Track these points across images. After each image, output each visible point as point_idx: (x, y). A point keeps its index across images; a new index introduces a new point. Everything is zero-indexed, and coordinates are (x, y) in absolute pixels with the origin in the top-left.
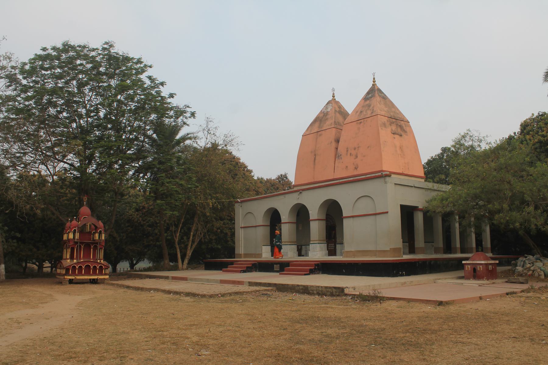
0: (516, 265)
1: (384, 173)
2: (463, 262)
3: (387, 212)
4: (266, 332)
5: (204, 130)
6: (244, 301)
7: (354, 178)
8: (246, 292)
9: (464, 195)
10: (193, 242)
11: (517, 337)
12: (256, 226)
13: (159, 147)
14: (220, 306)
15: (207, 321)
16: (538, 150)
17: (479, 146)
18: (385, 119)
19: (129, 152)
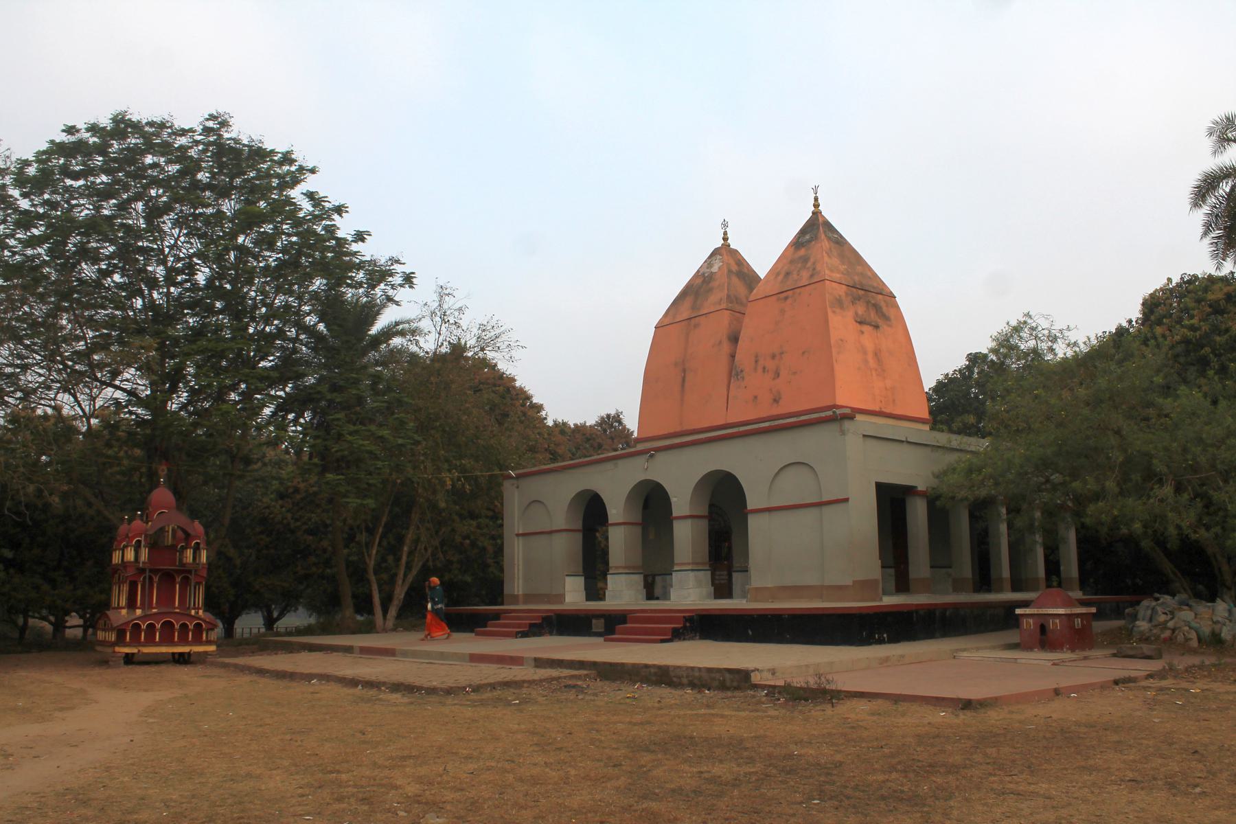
0: (1135, 617)
2: (1018, 611)
3: (846, 500)
4: (573, 772)
5: (433, 313)
6: (524, 701)
8: (529, 682)
10: (409, 567)
11: (1139, 779)
12: (551, 532)
13: (331, 352)
16: (1182, 360)
17: (1051, 350)
18: (841, 290)
19: (262, 364)
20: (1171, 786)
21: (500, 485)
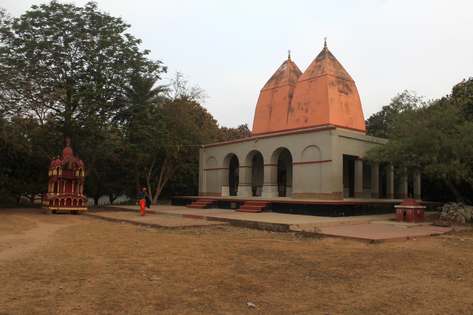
0: (441, 211)
1: (330, 126)
2: (395, 206)
3: (331, 161)
4: (214, 261)
5: (175, 83)
6: (201, 233)
7: (304, 130)
9: (399, 148)
10: (163, 181)
11: (437, 273)
12: (217, 169)
13: (135, 97)
14: (179, 237)
15: (165, 250)
16: (467, 111)
17: (415, 105)
18: (333, 79)
19: (108, 101)
20: (449, 277)
21: (199, 150)
